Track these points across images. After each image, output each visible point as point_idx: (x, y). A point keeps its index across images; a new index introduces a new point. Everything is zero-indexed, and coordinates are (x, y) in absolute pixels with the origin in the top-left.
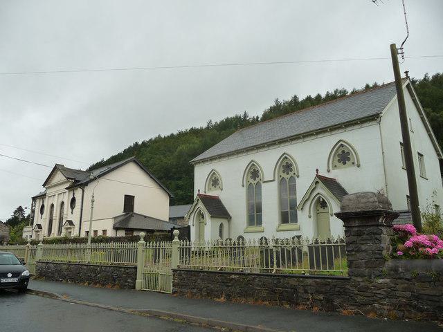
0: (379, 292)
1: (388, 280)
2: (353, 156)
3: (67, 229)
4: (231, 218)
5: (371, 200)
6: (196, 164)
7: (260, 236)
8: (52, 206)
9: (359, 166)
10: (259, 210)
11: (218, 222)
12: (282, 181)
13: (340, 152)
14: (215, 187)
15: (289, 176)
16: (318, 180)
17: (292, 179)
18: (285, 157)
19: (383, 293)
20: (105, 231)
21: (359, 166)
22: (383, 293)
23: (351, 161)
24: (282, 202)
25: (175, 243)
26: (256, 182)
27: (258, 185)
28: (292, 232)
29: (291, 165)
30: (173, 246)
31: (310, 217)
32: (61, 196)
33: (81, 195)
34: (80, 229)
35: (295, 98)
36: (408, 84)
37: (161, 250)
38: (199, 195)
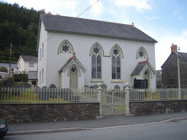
10: (119, 70)
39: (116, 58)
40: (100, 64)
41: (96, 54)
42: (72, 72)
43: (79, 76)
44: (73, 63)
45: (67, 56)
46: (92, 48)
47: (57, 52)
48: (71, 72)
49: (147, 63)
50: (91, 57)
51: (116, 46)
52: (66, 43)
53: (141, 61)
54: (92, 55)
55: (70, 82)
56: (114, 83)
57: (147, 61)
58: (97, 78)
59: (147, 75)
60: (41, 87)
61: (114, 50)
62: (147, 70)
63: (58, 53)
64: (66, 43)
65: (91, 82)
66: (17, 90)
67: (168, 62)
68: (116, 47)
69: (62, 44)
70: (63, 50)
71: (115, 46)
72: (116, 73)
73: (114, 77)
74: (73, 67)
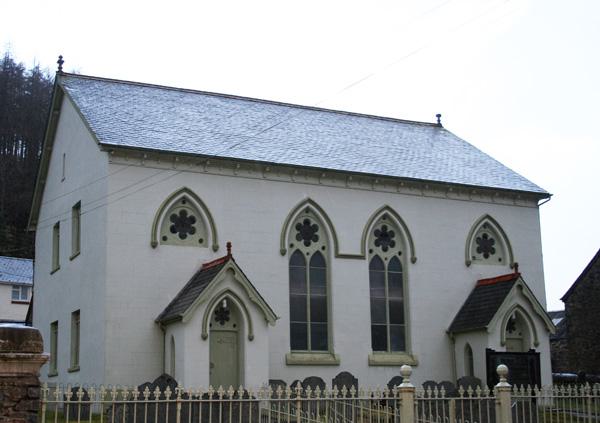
10: (399, 313)
39: (386, 263)
40: (325, 289)
41: (304, 250)
42: (217, 326)
43: (247, 341)
44: (222, 283)
45: (189, 258)
46: (290, 225)
47: (148, 239)
48: (214, 322)
49: (517, 283)
50: (285, 261)
51: (387, 215)
52: (184, 200)
53: (489, 277)
54: (290, 252)
55: (212, 366)
56: (380, 368)
57: (516, 276)
58: (312, 349)
59: (515, 334)
60: (551, 404)
61: (478, 238)
62: (516, 313)
63: (154, 245)
64: (184, 202)
65: (287, 365)
66: (165, 398)
67: (591, 277)
68: (385, 217)
69: (171, 204)
70: (173, 230)
71: (380, 216)
72: (388, 324)
73: (378, 343)
74: (221, 303)
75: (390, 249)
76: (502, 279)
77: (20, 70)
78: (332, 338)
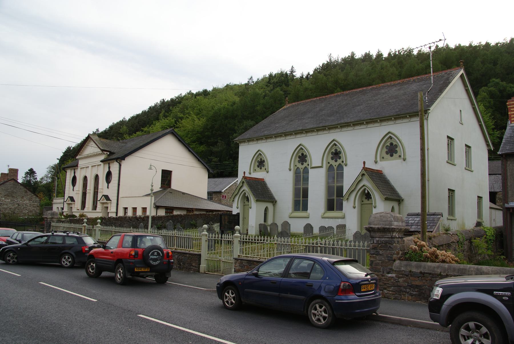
0: (388, 282)
1: (394, 275)
2: (399, 149)
3: (103, 203)
4: (276, 202)
5: (389, 219)
6: (241, 142)
7: (305, 222)
8: (85, 178)
9: (404, 160)
10: (306, 193)
11: (263, 206)
12: (330, 168)
13: (388, 144)
14: (261, 168)
15: (337, 164)
16: (364, 172)
17: (340, 167)
18: (334, 143)
19: (391, 283)
20: (144, 209)
21: (404, 160)
22: (391, 283)
23: (398, 154)
24: (329, 190)
25: (237, 237)
26: (303, 167)
27: (306, 171)
28: (337, 220)
29: (340, 152)
30: (235, 239)
31: (354, 208)
32: (95, 169)
33: (118, 169)
34: (117, 204)
35: (353, 54)
36: (462, 75)
37: (223, 241)
38: (244, 177)
75: (334, 161)
76: (256, 179)
77: (286, 73)
78: (455, 196)
